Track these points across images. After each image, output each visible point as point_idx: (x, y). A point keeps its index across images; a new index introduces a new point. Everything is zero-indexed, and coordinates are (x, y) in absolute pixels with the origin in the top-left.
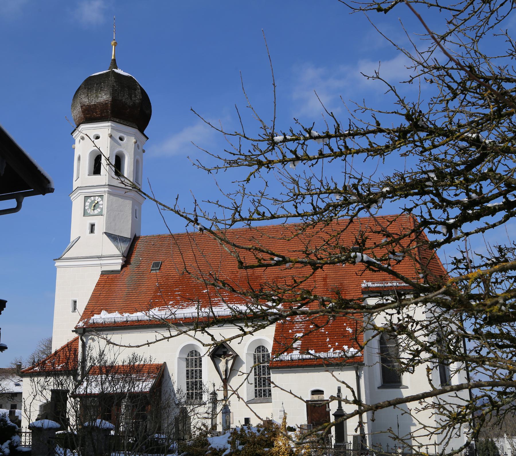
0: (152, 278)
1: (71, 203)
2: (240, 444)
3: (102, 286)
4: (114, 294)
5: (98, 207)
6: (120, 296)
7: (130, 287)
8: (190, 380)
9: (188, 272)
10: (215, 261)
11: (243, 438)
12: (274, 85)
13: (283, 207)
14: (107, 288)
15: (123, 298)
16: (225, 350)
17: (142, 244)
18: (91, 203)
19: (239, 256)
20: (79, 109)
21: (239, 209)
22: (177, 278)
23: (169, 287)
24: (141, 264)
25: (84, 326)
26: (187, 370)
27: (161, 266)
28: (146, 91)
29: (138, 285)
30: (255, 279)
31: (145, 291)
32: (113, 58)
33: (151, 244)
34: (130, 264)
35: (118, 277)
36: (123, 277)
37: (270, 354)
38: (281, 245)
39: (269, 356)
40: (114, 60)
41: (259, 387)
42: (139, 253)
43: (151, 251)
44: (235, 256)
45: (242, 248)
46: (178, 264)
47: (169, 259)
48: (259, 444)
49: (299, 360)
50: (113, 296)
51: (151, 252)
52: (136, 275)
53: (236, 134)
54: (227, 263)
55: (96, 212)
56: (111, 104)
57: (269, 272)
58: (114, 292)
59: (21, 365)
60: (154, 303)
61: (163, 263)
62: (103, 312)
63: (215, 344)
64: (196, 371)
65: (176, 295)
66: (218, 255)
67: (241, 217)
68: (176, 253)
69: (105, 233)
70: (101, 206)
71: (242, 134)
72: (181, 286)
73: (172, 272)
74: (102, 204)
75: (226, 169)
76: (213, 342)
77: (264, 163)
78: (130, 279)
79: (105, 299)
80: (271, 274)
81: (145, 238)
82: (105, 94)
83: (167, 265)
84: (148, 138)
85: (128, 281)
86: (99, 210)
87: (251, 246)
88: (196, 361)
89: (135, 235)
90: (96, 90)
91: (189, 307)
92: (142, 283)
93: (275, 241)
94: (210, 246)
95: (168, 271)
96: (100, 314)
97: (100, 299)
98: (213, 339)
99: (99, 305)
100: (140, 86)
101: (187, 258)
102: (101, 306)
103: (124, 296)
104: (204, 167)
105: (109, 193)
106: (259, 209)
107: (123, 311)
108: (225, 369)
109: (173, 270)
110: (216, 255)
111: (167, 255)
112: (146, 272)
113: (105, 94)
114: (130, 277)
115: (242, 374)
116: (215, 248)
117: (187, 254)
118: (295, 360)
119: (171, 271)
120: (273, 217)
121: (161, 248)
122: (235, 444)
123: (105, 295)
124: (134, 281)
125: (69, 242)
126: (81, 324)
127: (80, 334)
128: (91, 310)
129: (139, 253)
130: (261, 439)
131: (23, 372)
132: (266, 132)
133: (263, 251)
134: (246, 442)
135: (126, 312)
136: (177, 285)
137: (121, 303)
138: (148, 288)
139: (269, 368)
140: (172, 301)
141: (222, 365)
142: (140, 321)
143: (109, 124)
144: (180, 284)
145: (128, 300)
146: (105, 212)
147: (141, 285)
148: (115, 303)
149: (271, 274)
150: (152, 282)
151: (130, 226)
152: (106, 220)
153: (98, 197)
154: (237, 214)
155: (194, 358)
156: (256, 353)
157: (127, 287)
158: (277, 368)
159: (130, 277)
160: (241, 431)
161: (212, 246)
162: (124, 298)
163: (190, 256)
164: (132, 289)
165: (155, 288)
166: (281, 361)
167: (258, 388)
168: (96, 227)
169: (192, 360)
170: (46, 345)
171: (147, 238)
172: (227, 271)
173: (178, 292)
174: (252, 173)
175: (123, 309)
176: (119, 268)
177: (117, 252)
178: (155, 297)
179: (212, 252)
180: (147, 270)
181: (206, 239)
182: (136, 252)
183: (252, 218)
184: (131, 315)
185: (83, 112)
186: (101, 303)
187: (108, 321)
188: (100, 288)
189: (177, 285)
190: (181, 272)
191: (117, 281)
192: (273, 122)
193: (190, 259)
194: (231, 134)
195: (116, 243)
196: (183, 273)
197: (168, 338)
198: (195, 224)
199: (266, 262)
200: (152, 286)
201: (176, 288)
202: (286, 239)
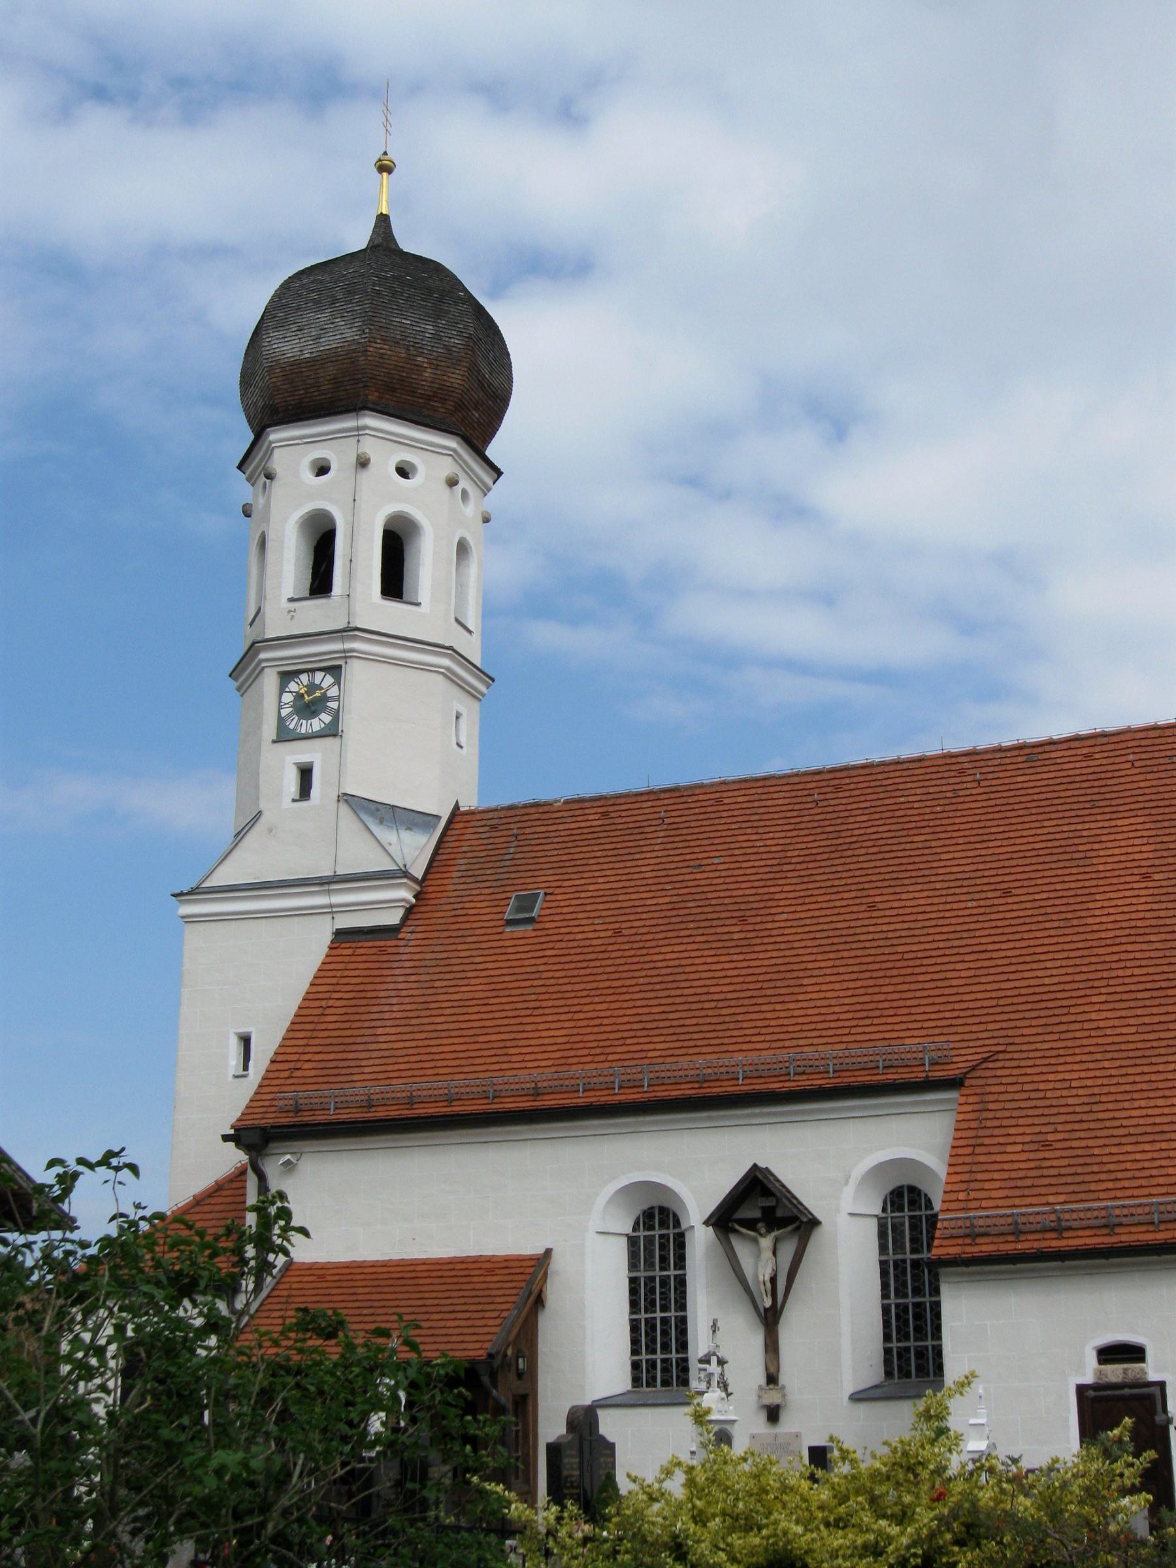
41: (898, 1340)
64: (664, 1282)
70: (333, 705)
74: (337, 698)
86: (326, 718)
89: (457, 807)
156: (889, 1214)
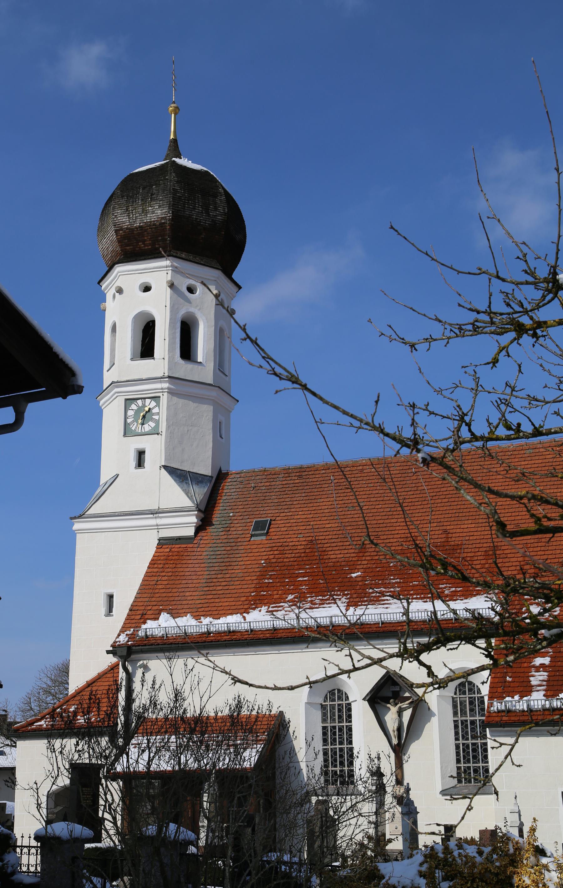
0: (254, 551)
1: (100, 412)
2: (445, 879)
3: (161, 566)
4: (184, 582)
5: (152, 419)
6: (194, 585)
7: (213, 568)
8: (329, 747)
9: (372, 542)
10: (373, 518)
11: (450, 866)
12: (557, 170)
13: (557, 413)
14: (169, 570)
15: (199, 589)
16: (397, 689)
17: (233, 487)
18: (137, 412)
19: (496, 512)
20: (111, 235)
21: (467, 419)
22: (301, 551)
23: (285, 568)
24: (232, 525)
25: (128, 641)
26: (324, 728)
27: (269, 528)
28: (234, 197)
29: (228, 564)
30: (451, 552)
31: (241, 575)
32: (172, 137)
33: (250, 486)
34: (211, 524)
35: (189, 550)
36: (199, 549)
37: (486, 699)
38: (500, 484)
39: (482, 702)
40: (175, 141)
42: (228, 504)
43: (251, 499)
44: (487, 511)
45: (506, 496)
46: (303, 524)
47: (284, 514)
48: (482, 881)
49: (545, 710)
50: (182, 586)
51: (250, 502)
52: (222, 545)
53: (479, 271)
54: (396, 520)
55: (147, 428)
56: (171, 225)
57: (478, 537)
58: (182, 578)
59: (6, 716)
60: (258, 598)
61: (273, 522)
62: (164, 616)
63: (437, 683)
64: (341, 729)
65: (300, 583)
66: (377, 507)
67: (472, 434)
68: (297, 502)
69: (165, 467)
70: (156, 417)
71: (493, 271)
72: (308, 565)
73: (291, 540)
74: (158, 414)
75: (448, 342)
76: (430, 680)
77: (528, 327)
78: (212, 553)
79: (167, 591)
80: (482, 541)
81: (238, 476)
82: (160, 207)
83: (280, 526)
84: (240, 287)
85: (209, 557)
86: (152, 424)
87: (524, 492)
88: (340, 711)
89: (220, 470)
90: (142, 200)
91: (325, 605)
92: (235, 559)
93: (488, 478)
94: (362, 489)
95: (283, 537)
96: (158, 619)
97: (157, 591)
98: (430, 673)
99: (155, 603)
100: (223, 188)
101: (319, 511)
102: (159, 603)
103: (201, 585)
104: (403, 339)
105: (171, 392)
106: (508, 416)
107: (201, 613)
108: (396, 725)
109: (293, 536)
110: (373, 507)
111: (280, 507)
112: (243, 540)
113: (160, 207)
114: (211, 549)
115: (498, 745)
116: (370, 492)
117: (318, 504)
118: (537, 711)
119: (289, 536)
120: (537, 432)
121: (268, 494)
122: (434, 877)
123: (166, 582)
124: (219, 557)
125: (98, 485)
126: (123, 639)
127: (121, 657)
128: (141, 612)
129: (228, 504)
130: (486, 869)
131: (17, 730)
132: (529, 267)
133: (547, 502)
134: (456, 875)
135: (205, 616)
136: (300, 563)
137: (195, 598)
138: (246, 570)
139: (484, 725)
140: (292, 594)
141: (391, 719)
142: (234, 632)
143: (165, 262)
144: (307, 562)
145: (209, 592)
146: (163, 427)
147: (233, 564)
148: (186, 598)
149: (482, 541)
150: (253, 558)
151: (209, 453)
152: (166, 442)
153: (150, 400)
154: (464, 428)
155: (336, 703)
157: (206, 569)
158: (501, 726)
159: (211, 549)
160: (443, 853)
161: (365, 489)
162: (202, 589)
163: (323, 507)
164: (217, 572)
165: (259, 570)
166: (509, 711)
167: (462, 765)
168: (147, 456)
169: (333, 707)
170: (53, 677)
171: (242, 475)
172: (396, 536)
173: (304, 577)
174: (503, 348)
175: (200, 610)
176: (190, 532)
177: (187, 503)
178: (260, 587)
179: (366, 500)
180: (243, 536)
181: (353, 476)
182: (221, 501)
183: (494, 437)
184: (216, 622)
185: (119, 241)
186: (160, 599)
187: (173, 632)
188: (156, 570)
189: (300, 563)
190: (359, 542)
191: (188, 558)
192: (555, 245)
193: (324, 515)
194: (469, 273)
195: (185, 485)
196: (363, 544)
197: (349, 672)
198: (413, 450)
199: (552, 524)
200: (254, 566)
201: (300, 569)
202: (557, 476)
